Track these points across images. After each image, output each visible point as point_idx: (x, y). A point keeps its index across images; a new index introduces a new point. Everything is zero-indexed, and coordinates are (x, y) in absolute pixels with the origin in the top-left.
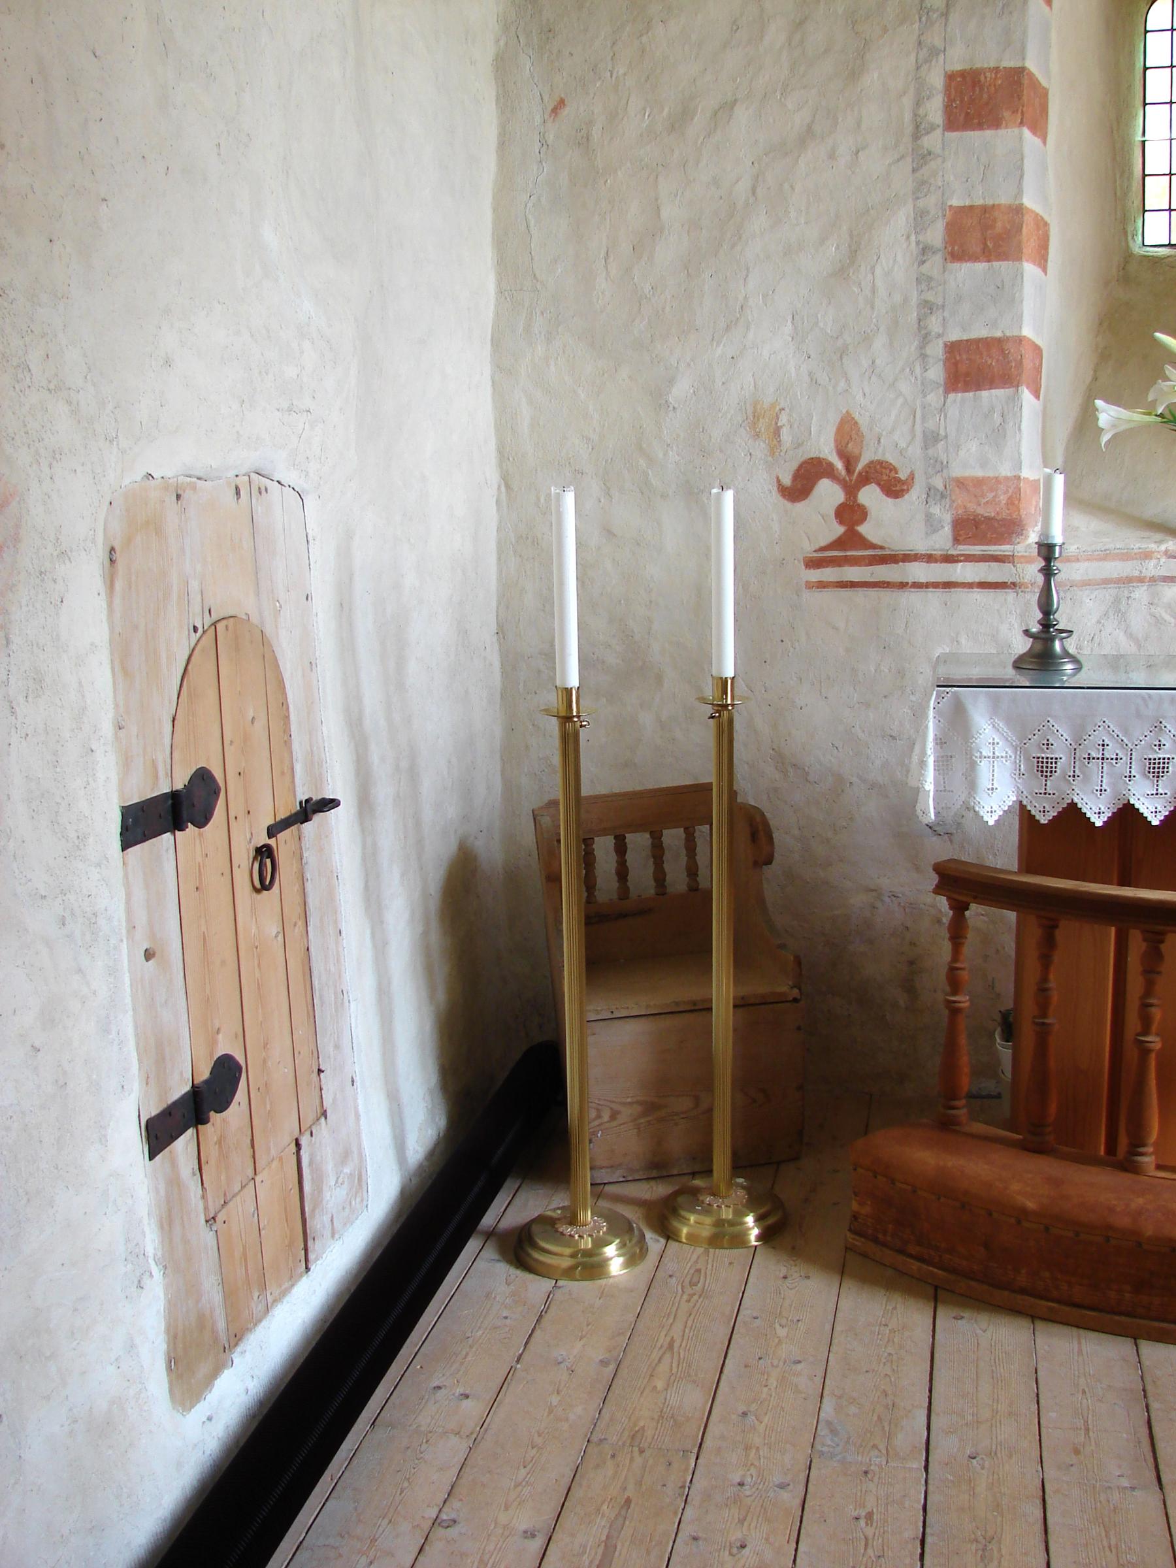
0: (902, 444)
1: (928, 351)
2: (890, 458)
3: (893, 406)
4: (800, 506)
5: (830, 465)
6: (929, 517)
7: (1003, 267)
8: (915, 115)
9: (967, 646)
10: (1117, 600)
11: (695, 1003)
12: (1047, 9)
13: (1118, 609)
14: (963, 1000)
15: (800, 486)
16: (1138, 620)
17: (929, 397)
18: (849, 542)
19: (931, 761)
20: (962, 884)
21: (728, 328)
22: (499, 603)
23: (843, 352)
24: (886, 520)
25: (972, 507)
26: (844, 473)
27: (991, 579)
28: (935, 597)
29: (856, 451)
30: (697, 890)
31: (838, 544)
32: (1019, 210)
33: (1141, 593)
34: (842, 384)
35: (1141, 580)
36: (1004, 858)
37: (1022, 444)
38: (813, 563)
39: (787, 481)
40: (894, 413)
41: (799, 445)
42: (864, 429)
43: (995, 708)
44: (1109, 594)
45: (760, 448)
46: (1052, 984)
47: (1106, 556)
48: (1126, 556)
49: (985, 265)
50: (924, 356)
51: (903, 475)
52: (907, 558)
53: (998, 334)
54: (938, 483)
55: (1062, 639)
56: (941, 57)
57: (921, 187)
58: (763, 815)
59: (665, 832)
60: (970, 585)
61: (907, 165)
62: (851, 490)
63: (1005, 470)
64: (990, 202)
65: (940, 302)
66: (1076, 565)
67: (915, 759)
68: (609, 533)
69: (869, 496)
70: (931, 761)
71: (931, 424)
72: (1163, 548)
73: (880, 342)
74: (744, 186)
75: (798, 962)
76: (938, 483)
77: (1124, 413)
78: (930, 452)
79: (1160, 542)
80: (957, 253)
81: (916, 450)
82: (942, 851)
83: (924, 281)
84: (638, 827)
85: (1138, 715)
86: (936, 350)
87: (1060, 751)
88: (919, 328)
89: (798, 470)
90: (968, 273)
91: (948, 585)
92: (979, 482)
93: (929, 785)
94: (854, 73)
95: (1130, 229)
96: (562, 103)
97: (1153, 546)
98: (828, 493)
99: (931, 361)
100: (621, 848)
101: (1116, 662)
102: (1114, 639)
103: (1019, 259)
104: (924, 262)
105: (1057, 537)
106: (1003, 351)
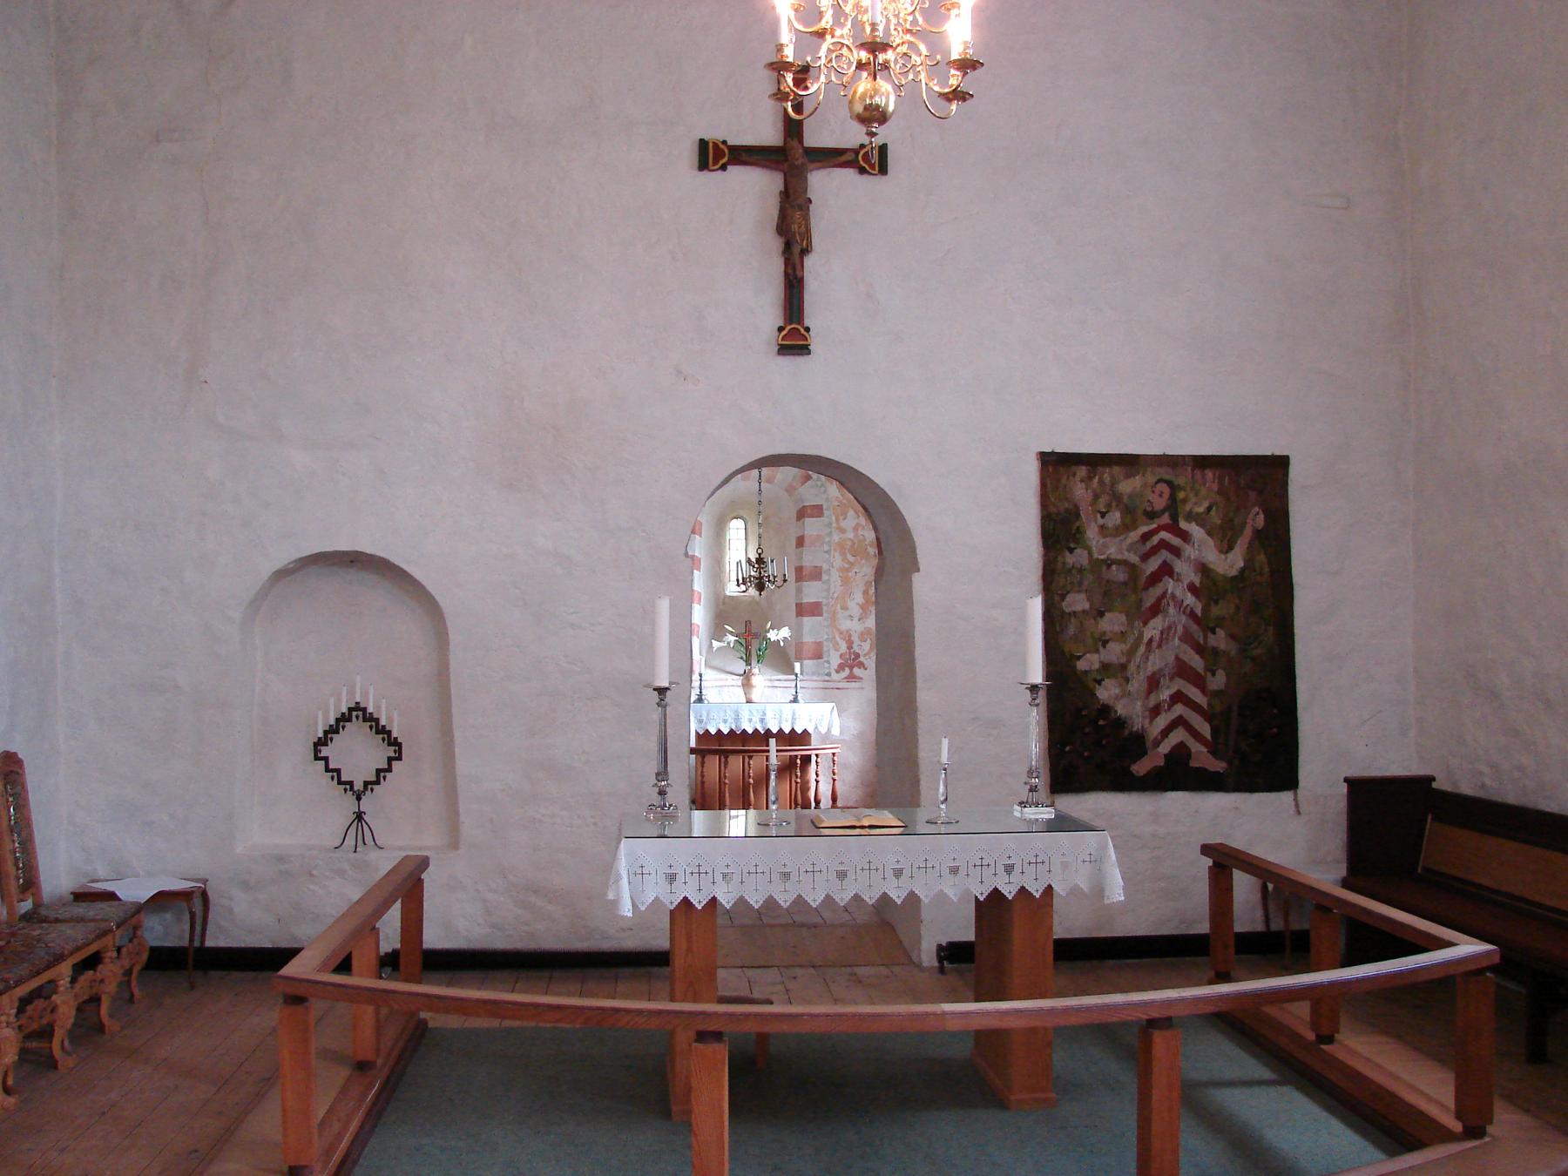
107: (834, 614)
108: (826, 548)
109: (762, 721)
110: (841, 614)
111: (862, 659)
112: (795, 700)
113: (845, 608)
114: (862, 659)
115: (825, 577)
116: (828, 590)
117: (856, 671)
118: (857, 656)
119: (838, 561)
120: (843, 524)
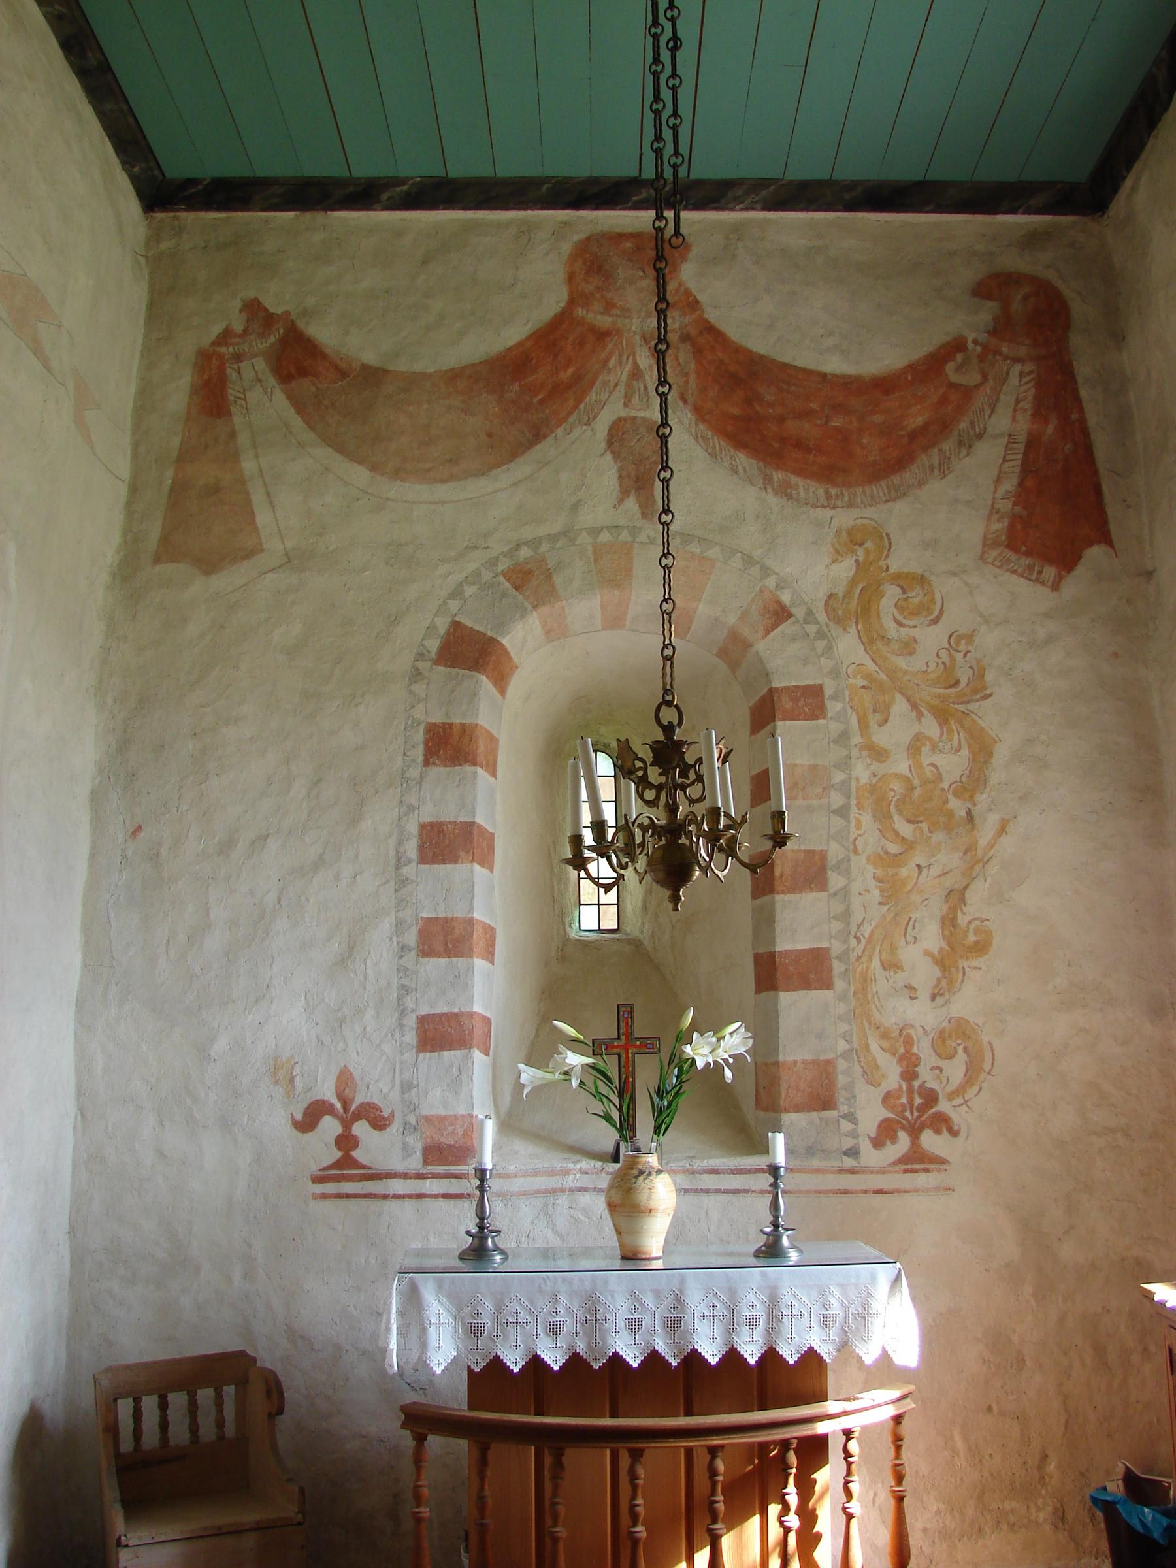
0: (385, 1091)
1: (405, 1022)
2: (376, 1100)
3: (379, 1063)
4: (308, 1136)
5: (332, 1105)
6: (405, 1146)
7: (459, 962)
8: (398, 852)
9: (434, 1243)
10: (546, 1206)
11: (220, 1528)
12: (492, 780)
13: (546, 1213)
14: (425, 1511)
15: (308, 1121)
16: (562, 1223)
17: (406, 1056)
18: (346, 1164)
19: (394, 1327)
20: (423, 1420)
21: (257, 1001)
22: (71, 1208)
23: (342, 1021)
24: (373, 1147)
25: (436, 1137)
26: (341, 1111)
27: (452, 1191)
28: (409, 1204)
29: (351, 1095)
30: (223, 1438)
31: (337, 1165)
32: (471, 921)
33: (563, 1200)
34: (341, 1045)
35: (563, 1191)
36: (456, 1399)
37: (473, 1091)
38: (318, 1180)
39: (299, 1116)
40: (379, 1066)
41: (309, 1090)
42: (357, 1077)
43: (440, 1285)
44: (539, 1201)
45: (279, 1092)
46: (487, 1492)
47: (536, 1173)
48: (551, 1173)
49: (446, 960)
50: (401, 1026)
51: (386, 1114)
52: (390, 1176)
53: (456, 1010)
54: (412, 1119)
55: (493, 1238)
56: (417, 812)
57: (400, 903)
58: (276, 1377)
59: (199, 1391)
60: (436, 1196)
61: (392, 885)
62: (347, 1124)
63: (461, 1110)
64: (450, 915)
65: (414, 986)
66: (514, 1180)
67: (383, 1327)
68: (161, 1154)
69: (361, 1129)
70: (394, 1327)
71: (406, 1076)
72: (578, 1166)
73: (370, 1013)
74: (271, 897)
75: (302, 1491)
76: (412, 1119)
77: (538, 1073)
78: (406, 1096)
79: (575, 1162)
80: (426, 951)
81: (395, 1095)
82: (411, 1397)
83: (402, 970)
84: (177, 1388)
85: (540, 1290)
86: (411, 1021)
87: (486, 1319)
88: (399, 1005)
89: (308, 1108)
90: (434, 966)
91: (420, 1196)
92: (442, 1119)
93: (393, 1346)
94: (355, 819)
95: (567, 921)
96: (140, 828)
97: (571, 1166)
98: (330, 1127)
99: (407, 1029)
100: (163, 1405)
101: (546, 1253)
102: (545, 1236)
103: (471, 957)
104: (402, 957)
105: (488, 1164)
106: (459, 1022)
107: (866, 980)
108: (837, 799)
109: (673, 1325)
110: (882, 983)
111: (944, 1106)
112: (771, 1252)
113: (892, 966)
114: (944, 1106)
115: (835, 881)
116: (846, 915)
117: (930, 1140)
118: (931, 1098)
119: (870, 837)
120: (881, 737)
